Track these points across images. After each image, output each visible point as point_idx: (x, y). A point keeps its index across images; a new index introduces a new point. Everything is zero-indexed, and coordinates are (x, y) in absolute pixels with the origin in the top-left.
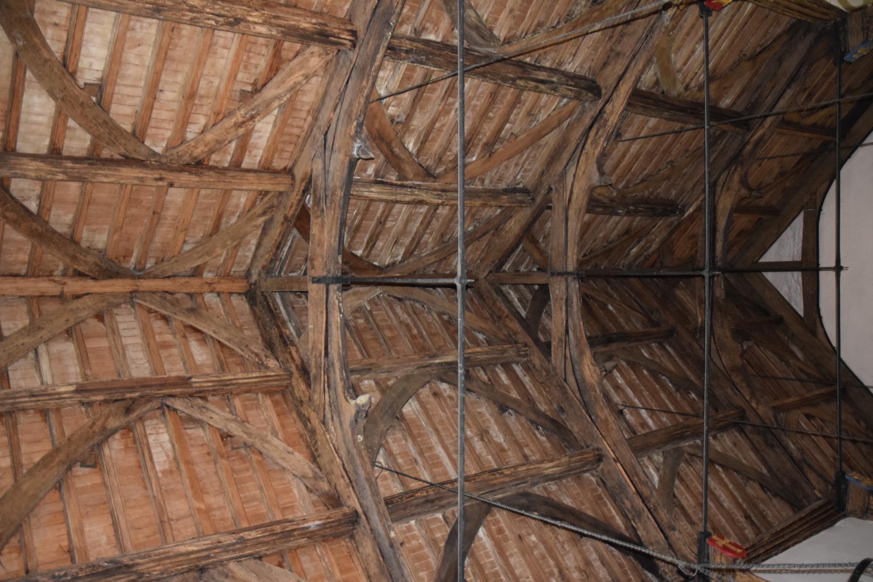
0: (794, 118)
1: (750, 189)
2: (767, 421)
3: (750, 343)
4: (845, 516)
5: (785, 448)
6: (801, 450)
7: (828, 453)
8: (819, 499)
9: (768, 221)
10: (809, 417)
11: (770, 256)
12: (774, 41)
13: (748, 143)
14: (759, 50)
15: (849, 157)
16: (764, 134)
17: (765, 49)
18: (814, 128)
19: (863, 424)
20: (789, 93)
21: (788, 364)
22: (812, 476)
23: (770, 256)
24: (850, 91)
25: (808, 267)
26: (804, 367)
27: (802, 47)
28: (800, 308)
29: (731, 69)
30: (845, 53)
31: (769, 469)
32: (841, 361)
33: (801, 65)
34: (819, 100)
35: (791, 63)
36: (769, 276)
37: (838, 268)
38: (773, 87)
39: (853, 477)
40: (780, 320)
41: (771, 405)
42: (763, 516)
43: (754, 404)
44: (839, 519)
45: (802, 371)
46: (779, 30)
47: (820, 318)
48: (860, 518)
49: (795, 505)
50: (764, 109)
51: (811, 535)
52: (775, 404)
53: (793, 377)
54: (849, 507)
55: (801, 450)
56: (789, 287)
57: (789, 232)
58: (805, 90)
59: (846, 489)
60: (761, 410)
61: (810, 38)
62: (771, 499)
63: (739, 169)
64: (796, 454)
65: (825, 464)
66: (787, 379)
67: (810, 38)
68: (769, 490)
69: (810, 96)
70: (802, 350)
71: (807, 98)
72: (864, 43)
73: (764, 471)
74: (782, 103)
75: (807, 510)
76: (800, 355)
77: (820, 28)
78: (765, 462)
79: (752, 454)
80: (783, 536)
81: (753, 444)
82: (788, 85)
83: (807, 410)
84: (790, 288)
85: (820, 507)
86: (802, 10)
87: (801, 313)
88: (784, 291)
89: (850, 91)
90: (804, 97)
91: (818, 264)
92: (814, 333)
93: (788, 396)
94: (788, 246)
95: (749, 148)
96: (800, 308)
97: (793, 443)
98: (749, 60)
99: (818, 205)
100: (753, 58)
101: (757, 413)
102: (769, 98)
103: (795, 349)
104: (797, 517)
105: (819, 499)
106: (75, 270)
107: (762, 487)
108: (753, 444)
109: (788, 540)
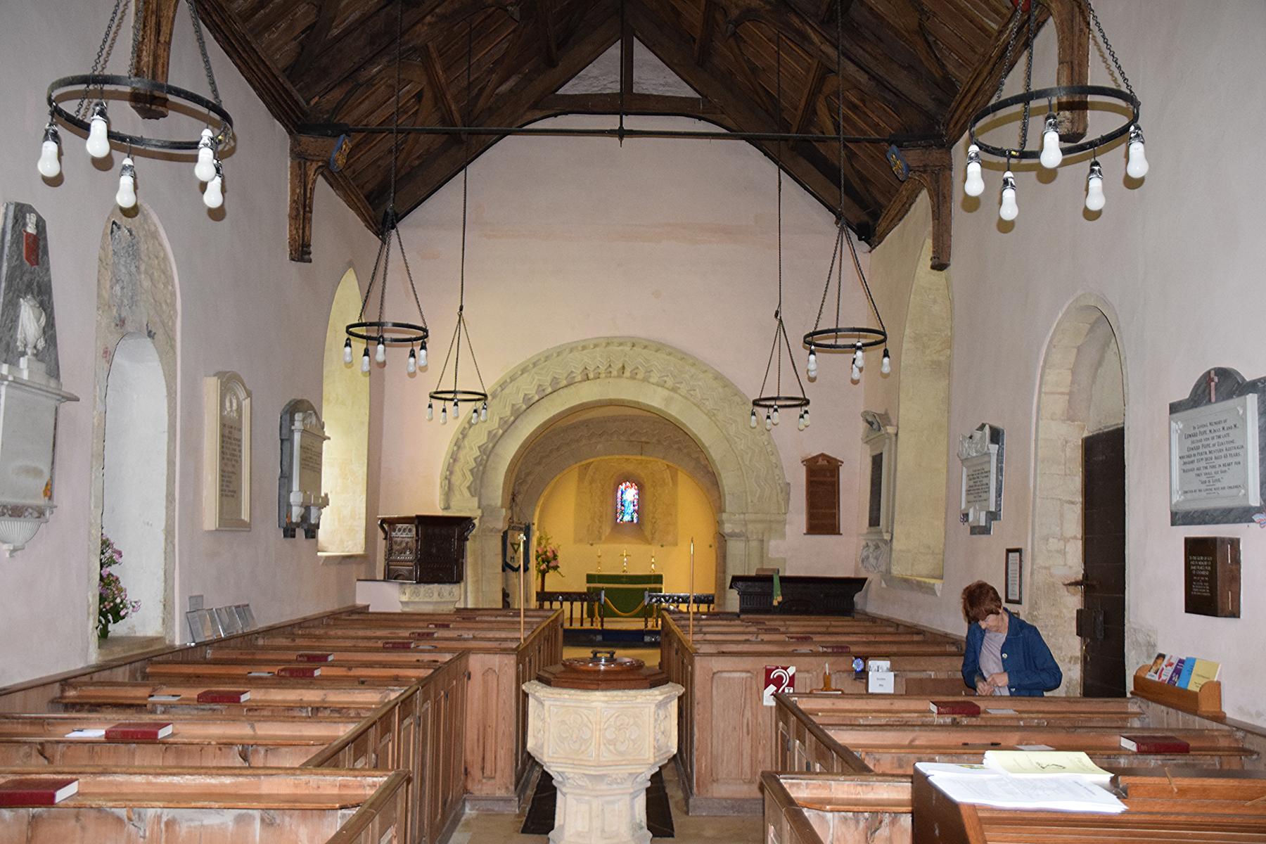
0: (828, 88)
1: (738, 23)
2: (406, 37)
3: (517, 16)
4: (290, 133)
5: (371, 61)
6: (370, 82)
7: (372, 118)
8: (308, 103)
9: (687, 55)
10: (419, 96)
11: (640, 51)
12: (938, 59)
13: (804, 21)
14: (931, 39)
15: (766, 154)
16: (812, 43)
17: (930, 47)
18: (811, 111)
19: (417, 162)
20: (863, 78)
21: (491, 71)
22: (337, 94)
23: (641, 52)
24: (851, 156)
25: (627, 101)
26: (488, 91)
27: (921, 96)
28: (568, 89)
29: (867, 72)
30: (900, 146)
31: (338, 39)
32: (504, 134)
33: (897, 94)
34: (846, 119)
35: (903, 82)
36: (615, 51)
37: (621, 133)
38: (875, 58)
39: (346, 144)
40: (551, 63)
41: (430, 44)
42: (268, 26)
43: (428, 18)
44: (286, 126)
45: (482, 90)
46: (950, 68)
47: (556, 115)
48: (292, 150)
49: (292, 71)
50: (848, 46)
51: (255, 89)
52: (432, 50)
53: (472, 78)
54: (304, 139)
55: (370, 82)
56: (600, 76)
57: (673, 78)
58: (863, 101)
59: (327, 135)
60: (422, 29)
61: (931, 106)
62: (295, 39)
63: (768, 7)
64: (365, 75)
65: (357, 113)
66: (469, 68)
67: (931, 106)
68: (307, 36)
69: (853, 107)
70: (511, 91)
71: (851, 103)
72: (908, 166)
73: (335, 32)
74: (851, 68)
75: (288, 85)
76: (504, 88)
77: (939, 117)
78: (347, 32)
79: (357, 14)
80: (244, 50)
81: (371, 17)
82: (872, 77)
83: (428, 95)
84: (596, 78)
85: (296, 103)
86: (970, 95)
87: (560, 92)
88: (592, 70)
89: (851, 156)
90: (853, 99)
91: (627, 114)
92: (535, 106)
93: (446, 69)
94: (655, 76)
95: (796, 21)
96: (568, 89)
97: (380, 71)
98: (920, 25)
99: (707, 116)
100: (922, 30)
101: (418, 22)
102: (861, 51)
103: (511, 83)
104: (276, 72)
105: (308, 103)
106: (519, 493)
107: (311, 27)
108: (371, 17)
109: (240, 57)
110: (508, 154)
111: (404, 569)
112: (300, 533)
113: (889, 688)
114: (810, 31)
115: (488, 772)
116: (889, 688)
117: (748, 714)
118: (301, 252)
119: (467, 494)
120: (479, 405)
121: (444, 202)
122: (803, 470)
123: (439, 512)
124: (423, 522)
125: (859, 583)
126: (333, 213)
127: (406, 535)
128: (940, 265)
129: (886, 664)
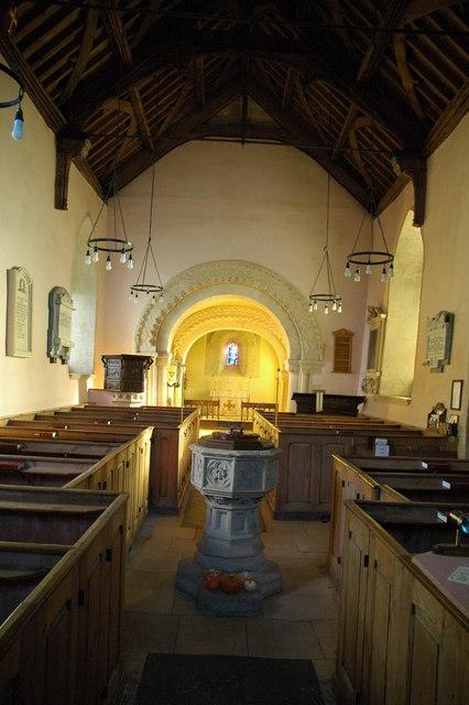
94: (257, 113)
110: (285, 150)
111: (115, 384)
112: (59, 361)
113: (386, 454)
114: (7, 65)
115: (163, 494)
116: (386, 454)
117: (308, 466)
118: (61, 203)
119: (149, 344)
120: (156, 294)
121: (141, 183)
122: (333, 337)
123: (134, 353)
124: (126, 358)
125: (362, 400)
126: (79, 185)
127: (116, 367)
128: (419, 221)
129: (385, 441)
